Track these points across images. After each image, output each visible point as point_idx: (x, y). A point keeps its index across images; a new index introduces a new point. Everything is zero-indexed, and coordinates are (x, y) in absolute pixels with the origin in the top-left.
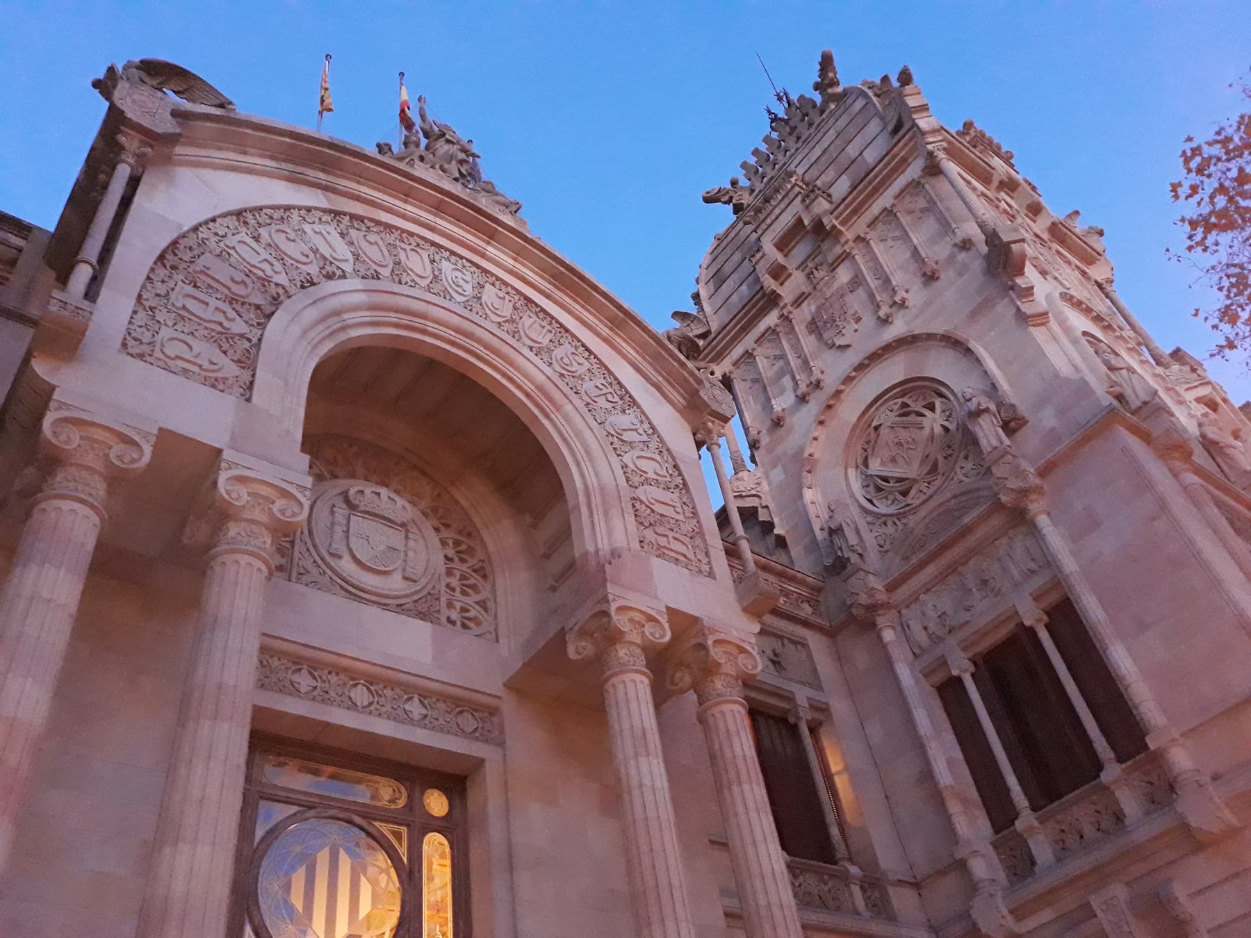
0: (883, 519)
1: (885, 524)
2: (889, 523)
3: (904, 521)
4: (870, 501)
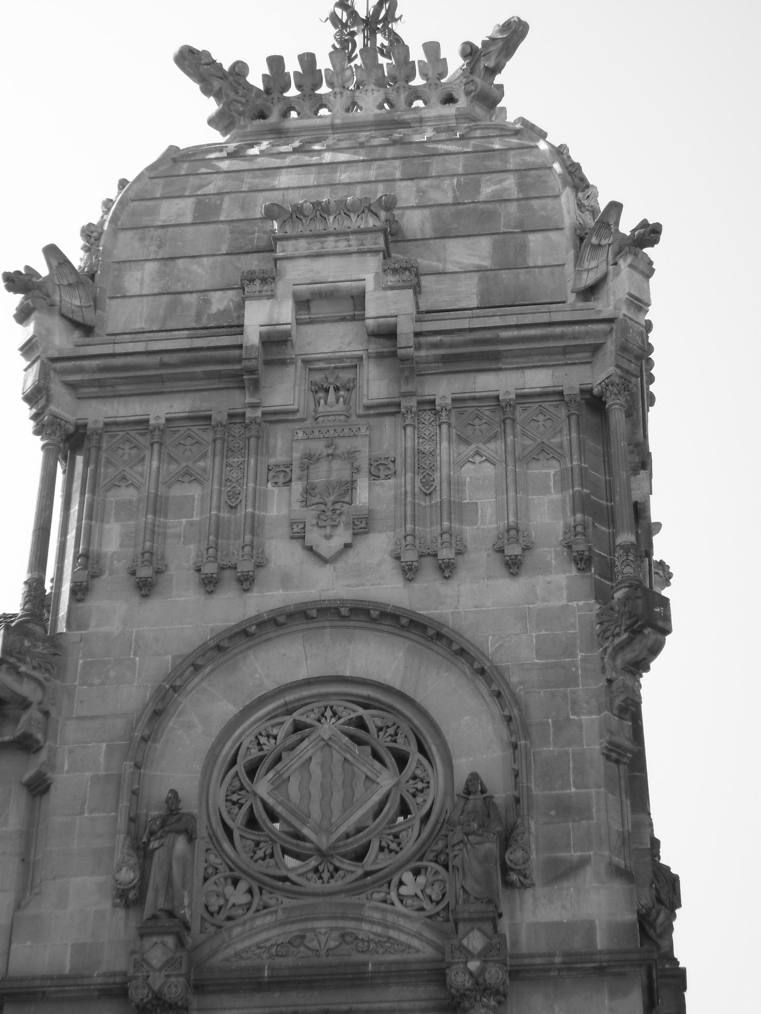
0: (237, 873)
1: (235, 882)
2: (243, 886)
3: (266, 897)
4: (229, 832)
